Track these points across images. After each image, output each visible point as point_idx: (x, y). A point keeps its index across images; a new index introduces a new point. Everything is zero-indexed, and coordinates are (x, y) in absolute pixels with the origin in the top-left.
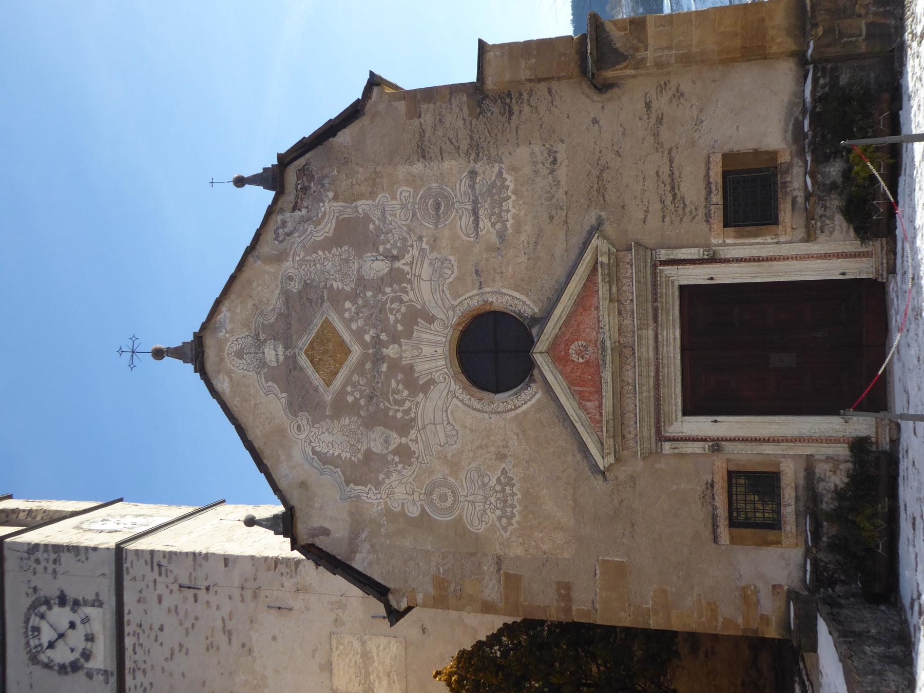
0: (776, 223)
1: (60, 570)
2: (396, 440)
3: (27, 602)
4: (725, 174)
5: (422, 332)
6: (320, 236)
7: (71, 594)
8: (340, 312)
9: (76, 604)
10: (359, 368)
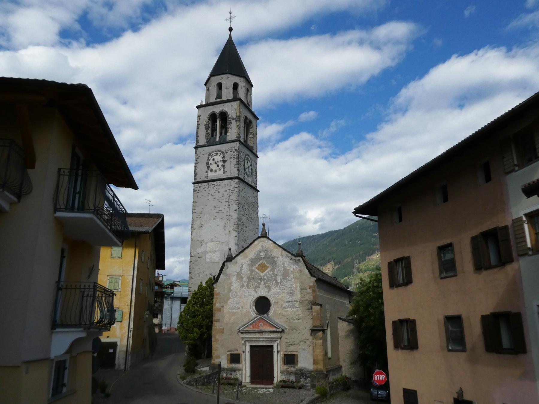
0: (285, 364)
1: (232, 160)
2: (245, 284)
3: (224, 151)
4: (294, 355)
5: (266, 289)
6: (286, 265)
7: (226, 164)
8: (270, 271)
9: (223, 166)
10: (259, 275)
